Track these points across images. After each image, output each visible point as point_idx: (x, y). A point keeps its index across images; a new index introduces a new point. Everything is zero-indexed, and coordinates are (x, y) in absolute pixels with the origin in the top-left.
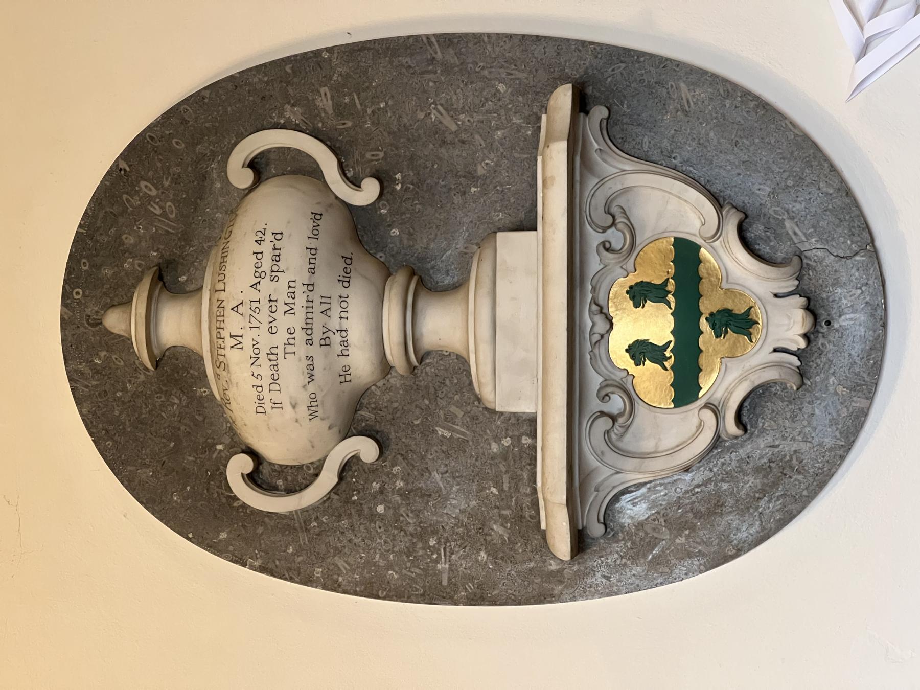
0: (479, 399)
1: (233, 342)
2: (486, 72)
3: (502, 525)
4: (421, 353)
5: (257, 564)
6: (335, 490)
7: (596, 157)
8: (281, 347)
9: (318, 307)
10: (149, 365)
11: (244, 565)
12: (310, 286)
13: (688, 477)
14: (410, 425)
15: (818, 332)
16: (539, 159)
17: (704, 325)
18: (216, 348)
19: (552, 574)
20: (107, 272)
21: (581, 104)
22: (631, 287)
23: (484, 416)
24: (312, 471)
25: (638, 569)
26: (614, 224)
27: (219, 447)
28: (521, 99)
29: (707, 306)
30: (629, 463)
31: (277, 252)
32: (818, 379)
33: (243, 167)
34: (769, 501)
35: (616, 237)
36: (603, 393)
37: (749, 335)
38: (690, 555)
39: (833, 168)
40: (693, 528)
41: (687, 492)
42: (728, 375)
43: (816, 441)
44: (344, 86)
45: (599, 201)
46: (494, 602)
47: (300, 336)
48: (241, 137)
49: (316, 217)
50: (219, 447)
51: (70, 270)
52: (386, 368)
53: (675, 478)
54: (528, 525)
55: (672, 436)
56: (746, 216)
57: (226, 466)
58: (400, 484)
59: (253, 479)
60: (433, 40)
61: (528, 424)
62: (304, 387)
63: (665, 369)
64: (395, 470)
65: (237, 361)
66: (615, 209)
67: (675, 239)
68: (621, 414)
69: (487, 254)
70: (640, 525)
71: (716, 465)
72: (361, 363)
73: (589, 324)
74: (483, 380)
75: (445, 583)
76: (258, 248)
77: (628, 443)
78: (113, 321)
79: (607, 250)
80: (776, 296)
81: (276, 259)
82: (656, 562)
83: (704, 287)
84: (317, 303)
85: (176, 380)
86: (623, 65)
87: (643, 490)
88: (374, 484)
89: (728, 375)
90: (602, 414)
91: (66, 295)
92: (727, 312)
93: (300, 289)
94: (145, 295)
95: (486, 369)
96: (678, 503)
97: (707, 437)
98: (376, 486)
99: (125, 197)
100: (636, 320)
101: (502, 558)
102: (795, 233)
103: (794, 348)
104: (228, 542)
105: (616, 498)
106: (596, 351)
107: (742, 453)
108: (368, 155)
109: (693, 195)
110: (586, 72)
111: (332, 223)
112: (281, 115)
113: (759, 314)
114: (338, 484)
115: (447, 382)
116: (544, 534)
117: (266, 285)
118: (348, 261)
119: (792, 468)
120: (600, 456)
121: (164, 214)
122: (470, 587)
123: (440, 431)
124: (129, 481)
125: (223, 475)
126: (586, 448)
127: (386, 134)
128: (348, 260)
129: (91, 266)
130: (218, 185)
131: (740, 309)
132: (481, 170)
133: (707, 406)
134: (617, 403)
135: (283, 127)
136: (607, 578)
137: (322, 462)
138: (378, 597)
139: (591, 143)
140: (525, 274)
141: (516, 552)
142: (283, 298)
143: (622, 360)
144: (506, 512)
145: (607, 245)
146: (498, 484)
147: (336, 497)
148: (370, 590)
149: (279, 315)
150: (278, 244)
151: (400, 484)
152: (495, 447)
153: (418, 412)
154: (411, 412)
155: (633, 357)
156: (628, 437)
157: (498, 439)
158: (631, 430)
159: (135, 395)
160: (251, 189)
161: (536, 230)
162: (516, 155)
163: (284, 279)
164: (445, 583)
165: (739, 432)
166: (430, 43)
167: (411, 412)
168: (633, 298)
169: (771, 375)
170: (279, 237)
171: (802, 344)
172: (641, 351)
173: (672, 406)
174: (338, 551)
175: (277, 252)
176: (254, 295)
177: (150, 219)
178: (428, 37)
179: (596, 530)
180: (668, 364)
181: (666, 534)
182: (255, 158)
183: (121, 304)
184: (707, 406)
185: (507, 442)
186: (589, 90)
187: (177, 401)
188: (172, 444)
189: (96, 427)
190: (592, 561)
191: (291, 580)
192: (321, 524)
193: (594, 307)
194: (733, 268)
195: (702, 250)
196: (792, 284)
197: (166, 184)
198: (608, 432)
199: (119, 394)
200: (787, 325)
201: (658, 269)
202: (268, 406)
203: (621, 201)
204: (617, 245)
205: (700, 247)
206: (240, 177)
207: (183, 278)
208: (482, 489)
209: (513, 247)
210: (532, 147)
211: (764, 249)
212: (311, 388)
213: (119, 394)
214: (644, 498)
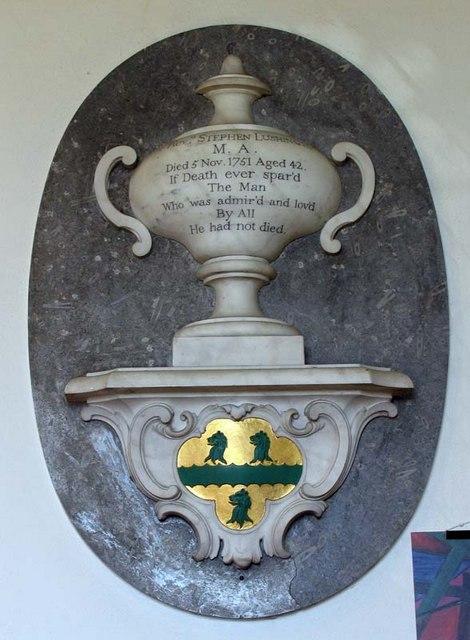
0: (181, 327)
1: (219, 146)
2: (420, 328)
3: (88, 346)
4: (213, 285)
5: (55, 170)
6: (112, 225)
7: (360, 408)
8: (215, 181)
9: (246, 207)
10: (200, 88)
11: (55, 160)
12: (261, 202)
13: (127, 480)
14: (160, 279)
15: (235, 571)
16: (358, 365)
17: (239, 488)
18: (215, 136)
19: (53, 383)
20: (267, 57)
21: (399, 396)
22: (265, 434)
23: (167, 330)
24: (125, 208)
25: (57, 445)
26: (312, 420)
27: (141, 141)
28: (402, 354)
29: (253, 490)
30: (136, 435)
31: (285, 177)
32: (201, 572)
33: (347, 153)
34: (110, 539)
35: (302, 422)
36: (187, 415)
37: (232, 521)
38: (69, 482)
39: (355, 580)
40: (89, 484)
41: (115, 479)
42: (208, 503)
43: (155, 571)
44: (408, 226)
45: (329, 410)
46: (31, 341)
47: (224, 195)
48: (369, 152)
49: (312, 206)
50: (141, 141)
51: (268, 31)
52: (202, 260)
53: (126, 471)
54: (88, 364)
55: (159, 466)
56: (319, 518)
57: (128, 145)
58: (117, 272)
59: (118, 165)
60: (444, 290)
61: (164, 360)
62: (188, 199)
63: (206, 460)
64: (127, 268)
65: (207, 150)
66: (322, 421)
67: (301, 466)
68: (172, 429)
69: (287, 331)
70: (90, 446)
71: (136, 500)
72: (208, 241)
73: (238, 404)
74: (195, 329)
75: (44, 306)
76: (288, 163)
77: (151, 435)
78: (232, 62)
79: (292, 416)
80: (261, 541)
81: (280, 177)
82: (63, 458)
83: (267, 487)
84: (249, 207)
85: (189, 109)
86: (427, 428)
87: (116, 448)
88: (116, 253)
89: (208, 503)
90: (173, 415)
91: (249, 28)
92: (248, 505)
93: (259, 194)
94: (252, 84)
95: (204, 331)
96: (108, 474)
97: (156, 491)
98: (115, 255)
99: (323, 69)
100: (241, 438)
101: (64, 347)
102: (307, 554)
103: (224, 553)
104: (71, 148)
105: (110, 428)
106: (218, 409)
107: (145, 519)
108: (357, 244)
109: (334, 478)
110: (422, 401)
111: (307, 218)
112: (385, 181)
113: (247, 526)
114: (116, 227)
115: (192, 305)
116: (83, 375)
117: (260, 170)
118: (279, 230)
119: (135, 555)
120: (141, 414)
121: (310, 97)
122: (42, 325)
123: (156, 301)
124: (114, 76)
125: (120, 143)
126: (147, 404)
127: (374, 257)
128: (280, 230)
129: (271, 46)
130: (333, 136)
131: (251, 514)
132: (347, 326)
133: (179, 491)
134: (180, 425)
135: (376, 183)
136: (51, 423)
137: (132, 215)
138: (33, 257)
139: (370, 404)
140: (270, 352)
141: (69, 357)
142: (252, 182)
143: (213, 428)
144: (98, 350)
145: (295, 417)
146: (118, 343)
147: (106, 226)
148: (37, 252)
149: (240, 179)
150: (291, 178)
151: (117, 272)
152: (145, 340)
153: (170, 284)
154: (174, 281)
155: (214, 436)
156: (155, 435)
157: (152, 341)
158: (160, 437)
159: (177, 80)
160: (331, 160)
161: (306, 363)
162: (360, 352)
163: (266, 182)
164: (44, 306)
165: (161, 516)
166: (440, 288)
167: (174, 281)
168: (257, 435)
169: (203, 538)
170: (296, 178)
171: (226, 560)
172: (219, 442)
173: (179, 466)
174: (66, 228)
175: (285, 177)
176: (254, 161)
177: (313, 92)
178: (445, 286)
179: (86, 414)
180: (210, 462)
181: (84, 465)
182: (354, 162)
183: (244, 68)
184: (179, 491)
185: (150, 348)
186: (408, 403)
187: (174, 109)
188: (142, 107)
189: (154, 52)
190: (63, 412)
191: (44, 195)
192: (86, 215)
193: (250, 408)
194: (277, 508)
195: (293, 487)
196: (269, 551)
197: (333, 99)
198: (159, 419)
199: (178, 67)
200: (240, 546)
201: (277, 455)
202: (172, 173)
203: (328, 427)
204: (296, 423)
205: (296, 484)
206: (339, 152)
207: (264, 112)
208: (114, 332)
209: (292, 347)
210: (367, 361)
211: (294, 533)
212: (187, 205)
213: (178, 67)
214: (110, 448)
